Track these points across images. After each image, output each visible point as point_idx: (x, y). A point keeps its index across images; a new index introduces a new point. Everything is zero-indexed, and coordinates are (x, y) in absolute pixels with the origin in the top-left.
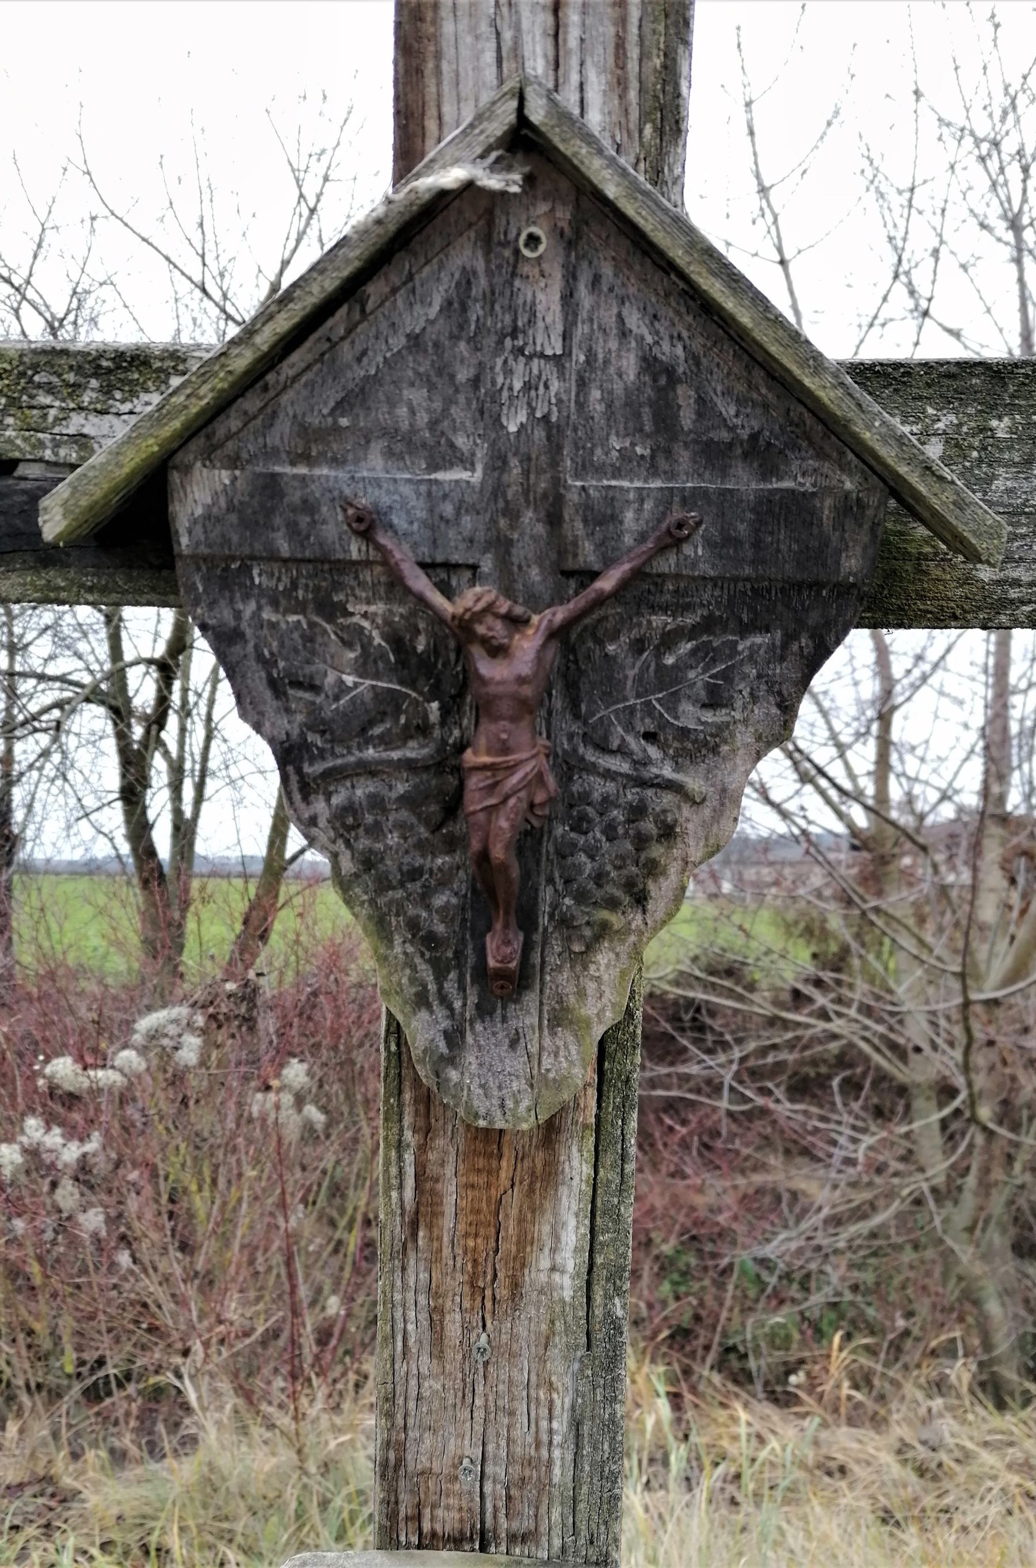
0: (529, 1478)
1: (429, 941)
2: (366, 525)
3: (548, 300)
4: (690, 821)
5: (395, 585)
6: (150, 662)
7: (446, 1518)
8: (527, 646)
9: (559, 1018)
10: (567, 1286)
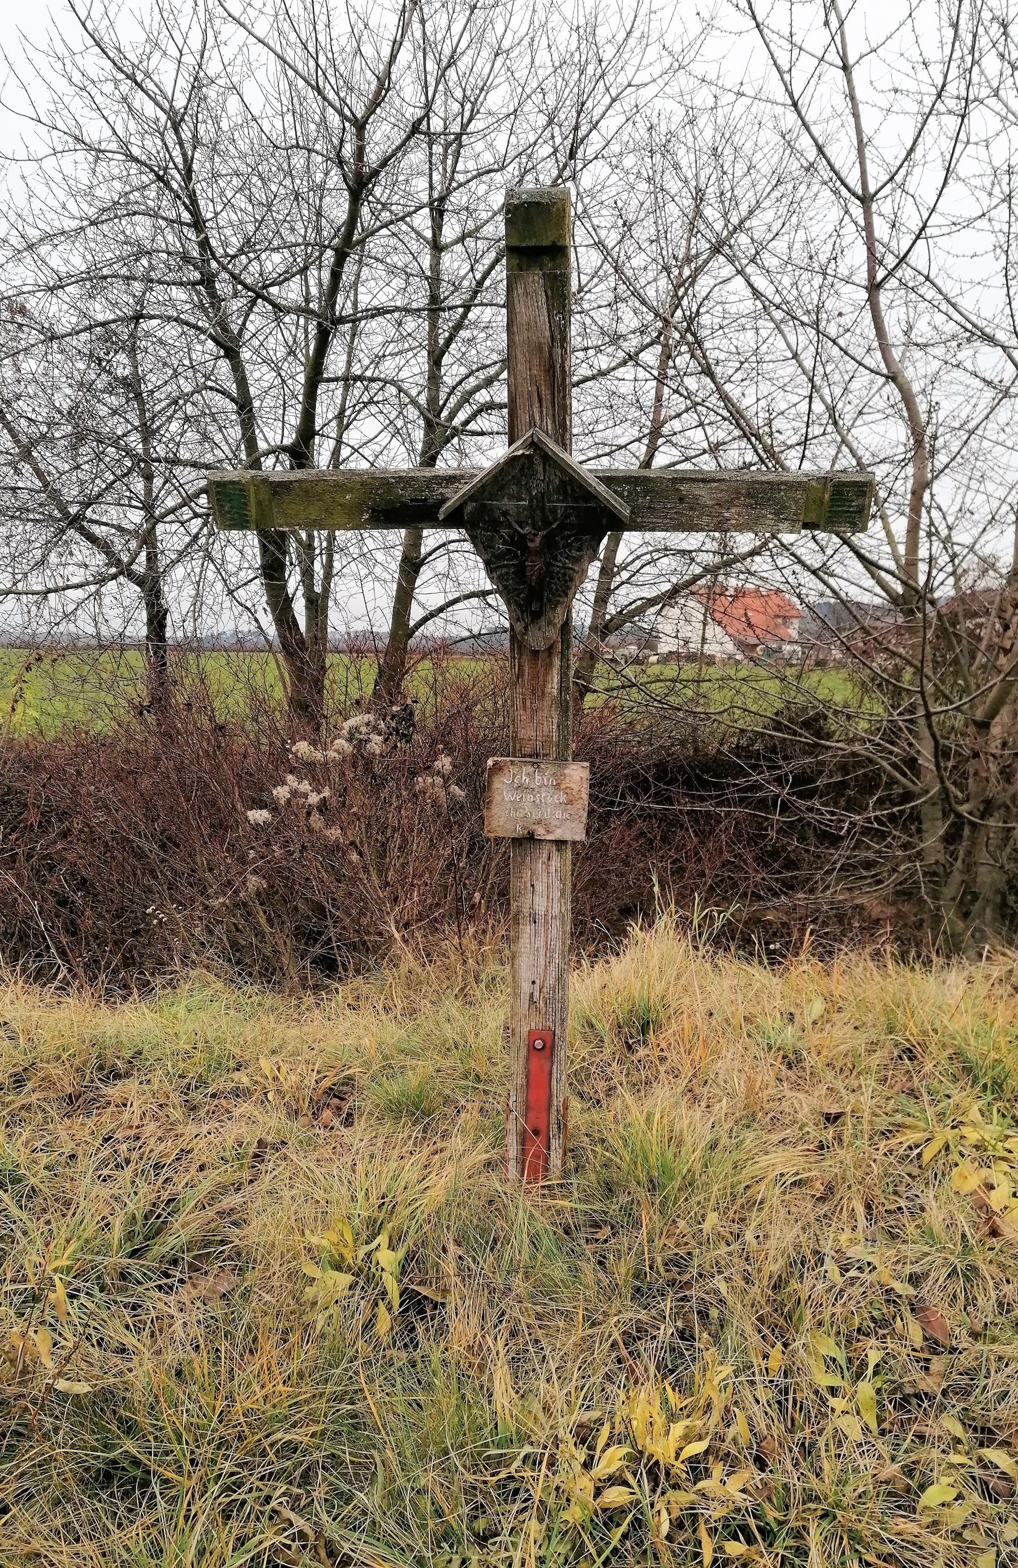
0: (547, 741)
1: (519, 606)
2: (505, 514)
3: (540, 469)
4: (576, 577)
5: (510, 527)
6: (284, 449)
7: (528, 750)
8: (538, 540)
9: (550, 623)
10: (555, 692)
